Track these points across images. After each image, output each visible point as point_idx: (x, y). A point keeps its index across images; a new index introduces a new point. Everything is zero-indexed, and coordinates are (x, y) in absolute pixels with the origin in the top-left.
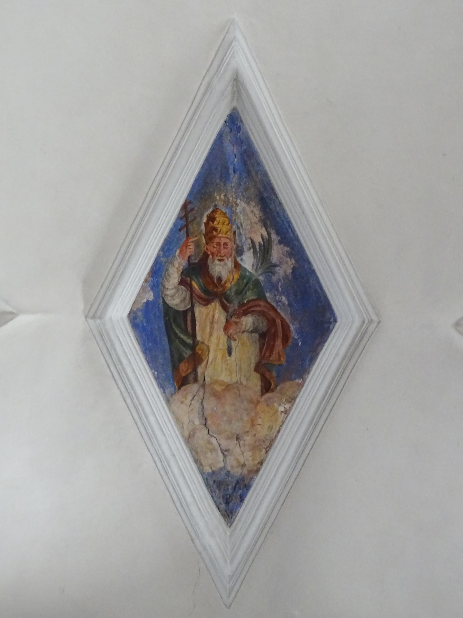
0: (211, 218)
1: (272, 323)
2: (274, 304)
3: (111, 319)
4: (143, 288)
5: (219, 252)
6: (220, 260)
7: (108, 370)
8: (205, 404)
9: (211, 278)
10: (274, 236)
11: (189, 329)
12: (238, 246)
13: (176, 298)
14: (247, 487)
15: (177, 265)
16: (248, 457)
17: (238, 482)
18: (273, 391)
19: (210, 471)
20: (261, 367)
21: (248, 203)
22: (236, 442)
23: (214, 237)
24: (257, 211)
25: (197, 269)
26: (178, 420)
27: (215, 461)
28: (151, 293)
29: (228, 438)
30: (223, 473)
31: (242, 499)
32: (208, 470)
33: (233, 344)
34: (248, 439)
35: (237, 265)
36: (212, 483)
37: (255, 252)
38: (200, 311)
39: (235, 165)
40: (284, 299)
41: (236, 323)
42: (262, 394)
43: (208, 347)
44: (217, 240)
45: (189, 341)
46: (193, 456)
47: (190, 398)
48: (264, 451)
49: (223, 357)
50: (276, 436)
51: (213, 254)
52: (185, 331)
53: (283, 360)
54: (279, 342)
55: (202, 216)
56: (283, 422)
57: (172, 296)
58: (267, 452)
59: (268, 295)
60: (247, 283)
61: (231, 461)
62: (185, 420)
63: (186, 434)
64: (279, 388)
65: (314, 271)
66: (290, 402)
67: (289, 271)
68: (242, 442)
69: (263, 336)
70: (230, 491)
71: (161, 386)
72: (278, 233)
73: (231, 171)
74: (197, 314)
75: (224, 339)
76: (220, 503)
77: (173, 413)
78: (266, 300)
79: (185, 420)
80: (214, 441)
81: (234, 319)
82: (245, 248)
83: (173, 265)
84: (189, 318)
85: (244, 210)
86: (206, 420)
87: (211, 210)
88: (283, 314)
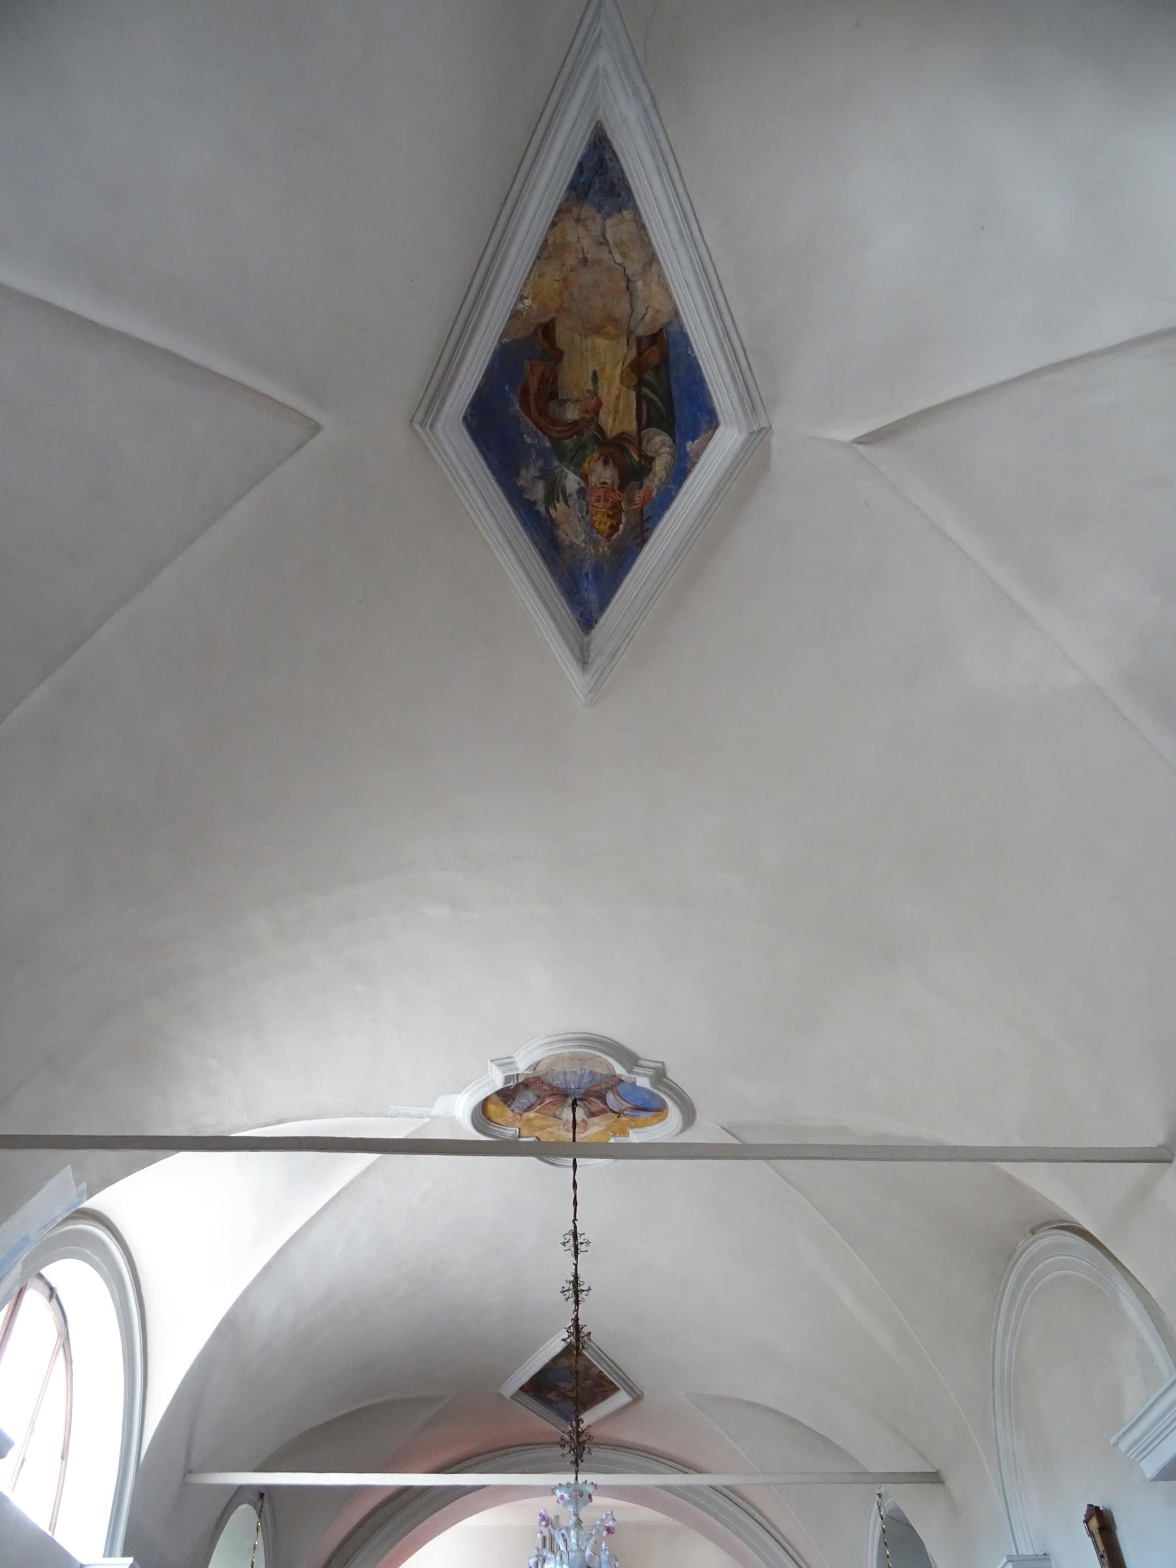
0: (614, 528)
1: (542, 412)
2: (540, 433)
3: (740, 432)
4: (698, 455)
5: (605, 492)
6: (604, 483)
7: (751, 361)
8: (629, 311)
9: (615, 464)
10: (542, 509)
11: (644, 406)
12: (584, 498)
13: (659, 443)
14: (573, 187)
15: (656, 480)
16: (572, 233)
17: (586, 194)
18: (540, 325)
19: (625, 213)
20: (554, 356)
21: (572, 543)
22: (589, 256)
23: (612, 508)
24: (561, 534)
25: (633, 473)
26: (666, 288)
27: (617, 229)
28: (688, 449)
29: (598, 262)
30: (607, 209)
31: (581, 167)
32: (627, 214)
33: (589, 386)
34: (571, 260)
35: (585, 477)
36: (623, 194)
37: (564, 492)
38: (630, 425)
39: (586, 581)
40: (528, 441)
41: (587, 412)
42: (553, 321)
43: (622, 382)
44: (609, 505)
45: (646, 391)
46: (647, 235)
47: (647, 317)
48: (550, 242)
49: (603, 370)
50: (534, 264)
51: (613, 490)
52: (650, 402)
53: (527, 365)
54: (533, 387)
55: (625, 530)
56: (525, 284)
57: (664, 445)
58: (546, 241)
59: (548, 444)
60: (573, 458)
61: (595, 229)
62: (655, 288)
63: (654, 268)
64: (532, 329)
65: (494, 473)
66: (517, 312)
67: (523, 472)
68: (580, 256)
69: (553, 395)
70: (596, 180)
71: (685, 336)
72: (538, 513)
73: (590, 576)
74: (635, 424)
75: (603, 392)
76: (611, 160)
77: (670, 297)
78: (551, 438)
79: (655, 288)
80: (618, 259)
81: (589, 416)
82: (575, 496)
83: (660, 480)
84: (644, 418)
85: (577, 537)
86: (628, 288)
87: (615, 536)
88: (529, 421)
